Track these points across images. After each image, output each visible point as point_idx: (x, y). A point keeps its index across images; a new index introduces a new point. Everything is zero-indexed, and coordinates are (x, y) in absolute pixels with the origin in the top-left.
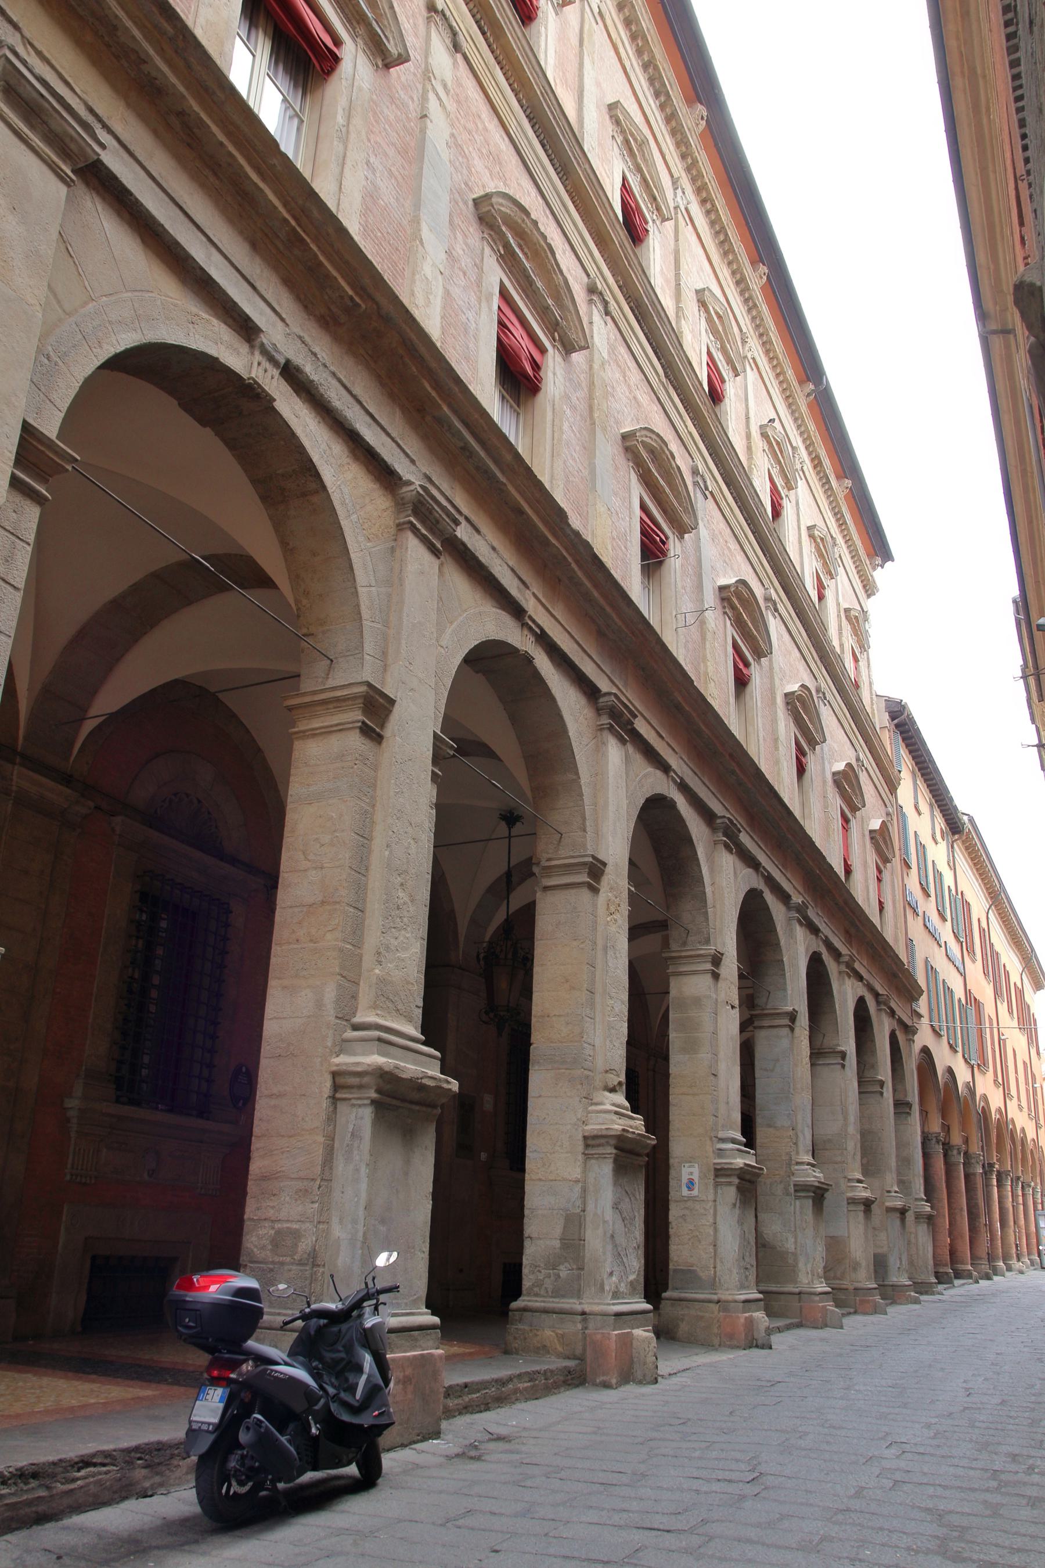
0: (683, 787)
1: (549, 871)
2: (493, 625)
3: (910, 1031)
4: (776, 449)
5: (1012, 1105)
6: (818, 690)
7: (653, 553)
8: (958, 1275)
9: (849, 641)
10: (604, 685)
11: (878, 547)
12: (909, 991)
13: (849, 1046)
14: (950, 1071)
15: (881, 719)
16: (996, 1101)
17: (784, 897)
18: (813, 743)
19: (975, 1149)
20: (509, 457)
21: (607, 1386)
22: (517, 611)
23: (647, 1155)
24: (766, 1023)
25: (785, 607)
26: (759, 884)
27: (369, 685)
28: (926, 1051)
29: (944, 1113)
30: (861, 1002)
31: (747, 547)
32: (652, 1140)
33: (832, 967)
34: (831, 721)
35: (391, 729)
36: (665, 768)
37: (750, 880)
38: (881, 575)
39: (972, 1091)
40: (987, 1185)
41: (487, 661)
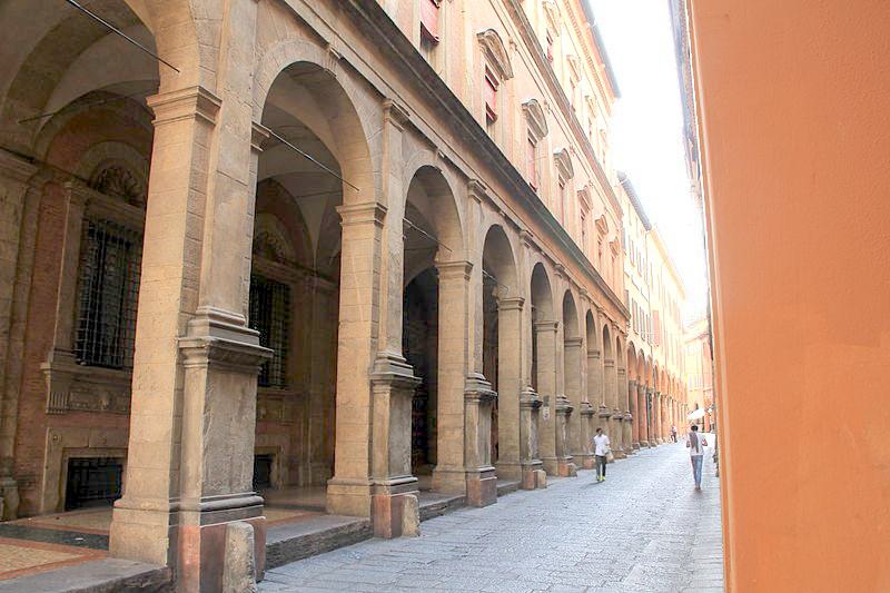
0: (507, 218)
1: (503, 303)
2: (298, 50)
3: (625, 335)
4: (572, 65)
5: (669, 362)
6: (571, 148)
7: (495, 104)
8: (642, 445)
9: (568, 74)
10: (471, 175)
11: (615, 93)
12: (625, 315)
13: (559, 318)
14: (642, 351)
15: (614, 183)
16: (661, 364)
17: (517, 229)
18: (542, 135)
19: (651, 386)
20: (465, 114)
21: (530, 489)
22: (323, 44)
23: (262, 366)
24: (542, 328)
25: (523, 48)
26: (498, 220)
27: (201, 89)
28: (632, 343)
29: (638, 371)
30: (589, 312)
31: (530, 67)
32: (269, 353)
33: (575, 295)
34: (519, 62)
35: (220, 119)
36: (433, 147)
37: (537, 258)
38: (616, 105)
39: (651, 359)
40: (656, 403)
41: (298, 76)
